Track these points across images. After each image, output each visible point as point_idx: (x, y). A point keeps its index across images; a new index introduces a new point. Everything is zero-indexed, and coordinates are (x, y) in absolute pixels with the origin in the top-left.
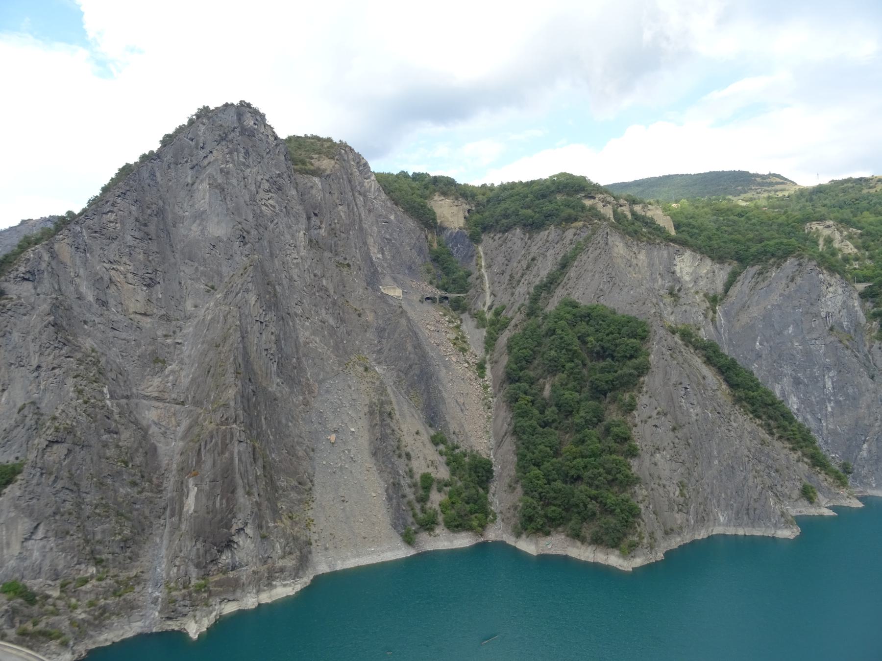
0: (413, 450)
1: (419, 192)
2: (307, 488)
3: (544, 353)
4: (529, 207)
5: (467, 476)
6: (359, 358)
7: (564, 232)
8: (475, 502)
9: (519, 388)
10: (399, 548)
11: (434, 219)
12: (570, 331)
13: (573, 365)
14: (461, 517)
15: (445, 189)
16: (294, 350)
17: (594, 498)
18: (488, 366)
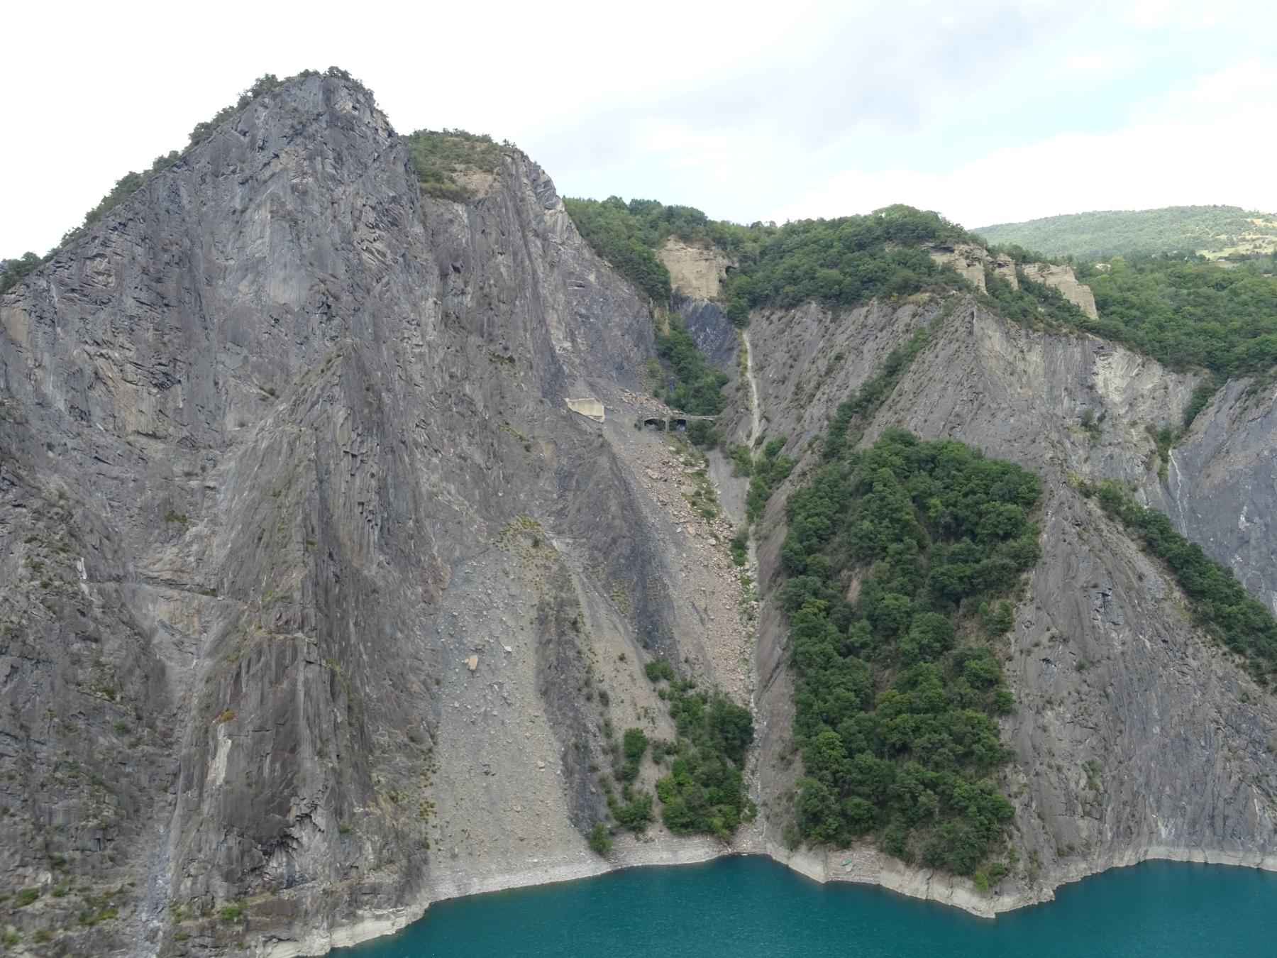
0: (613, 688)
1: (641, 234)
2: (424, 747)
3: (851, 524)
4: (835, 265)
5: (706, 737)
6: (524, 524)
7: (895, 310)
8: (719, 784)
9: (805, 585)
10: (581, 861)
11: (666, 283)
12: (899, 487)
13: (901, 546)
14: (692, 809)
15: (687, 229)
16: (411, 505)
17: (932, 785)
18: (751, 544)
